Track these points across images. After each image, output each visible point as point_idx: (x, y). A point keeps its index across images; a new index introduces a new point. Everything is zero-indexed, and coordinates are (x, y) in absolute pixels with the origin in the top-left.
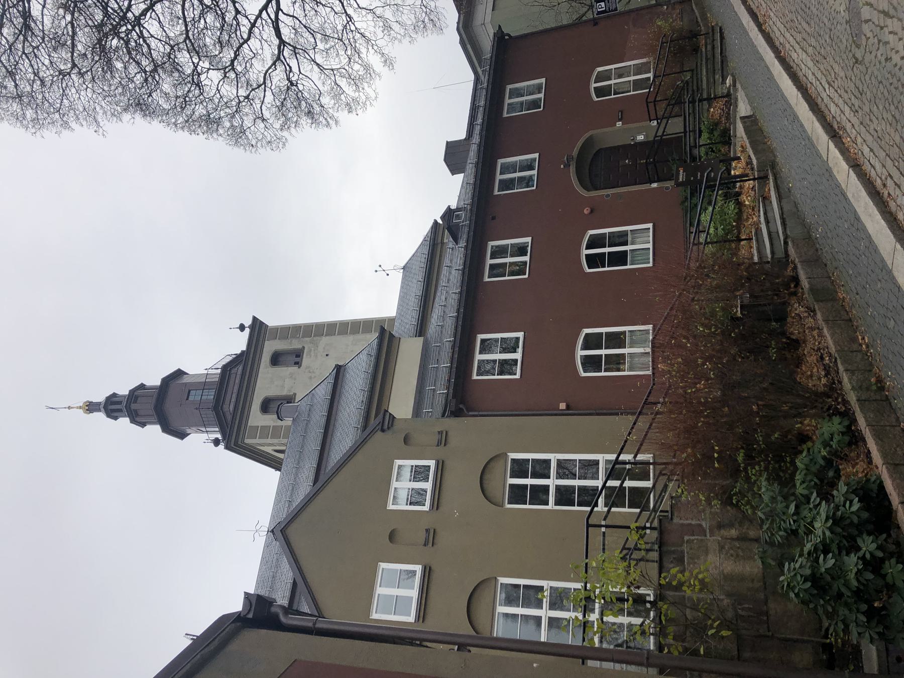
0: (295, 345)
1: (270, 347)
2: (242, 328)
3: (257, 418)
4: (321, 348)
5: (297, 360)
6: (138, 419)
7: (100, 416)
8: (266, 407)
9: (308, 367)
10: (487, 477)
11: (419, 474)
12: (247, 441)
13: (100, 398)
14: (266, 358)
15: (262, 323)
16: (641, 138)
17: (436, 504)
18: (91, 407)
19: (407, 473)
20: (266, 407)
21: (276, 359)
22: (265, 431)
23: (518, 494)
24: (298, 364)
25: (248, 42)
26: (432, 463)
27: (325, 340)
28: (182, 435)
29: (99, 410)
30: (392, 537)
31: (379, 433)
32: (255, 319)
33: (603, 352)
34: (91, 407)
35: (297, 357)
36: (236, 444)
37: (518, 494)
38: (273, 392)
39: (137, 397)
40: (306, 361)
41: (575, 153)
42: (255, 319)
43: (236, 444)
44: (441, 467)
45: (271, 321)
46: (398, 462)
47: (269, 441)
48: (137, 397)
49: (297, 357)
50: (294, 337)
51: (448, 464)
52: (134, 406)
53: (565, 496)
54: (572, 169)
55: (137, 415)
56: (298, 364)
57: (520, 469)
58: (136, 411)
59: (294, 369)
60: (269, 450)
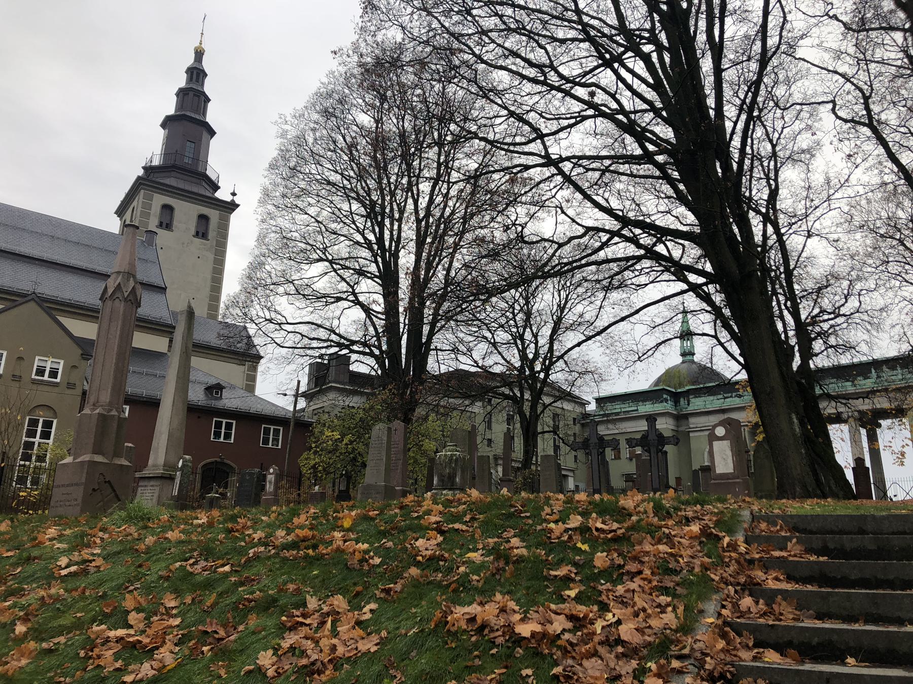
0: (212, 234)
1: (214, 215)
2: (234, 194)
3: (159, 200)
6: (182, 94)
7: (190, 60)
8: (168, 209)
11: (53, 374)
12: (142, 191)
13: (206, 65)
15: (234, 210)
16: (803, 451)
17: (34, 382)
18: (199, 54)
19: (55, 366)
21: (203, 218)
22: (147, 206)
23: (34, 423)
24: (197, 234)
25: (192, 378)
26: (58, 380)
27: (211, 256)
29: (196, 60)
30: (20, 358)
31: (80, 352)
32: (238, 206)
33: (223, 431)
34: (199, 54)
35: (202, 233)
37: (34, 423)
38: (177, 213)
39: (199, 97)
41: (226, 461)
42: (238, 206)
45: (235, 218)
46: (62, 362)
48: (199, 97)
49: (202, 233)
50: (219, 233)
51: (56, 389)
52: (191, 94)
56: (197, 234)
57: (48, 424)
59: (193, 232)
60: (135, 203)
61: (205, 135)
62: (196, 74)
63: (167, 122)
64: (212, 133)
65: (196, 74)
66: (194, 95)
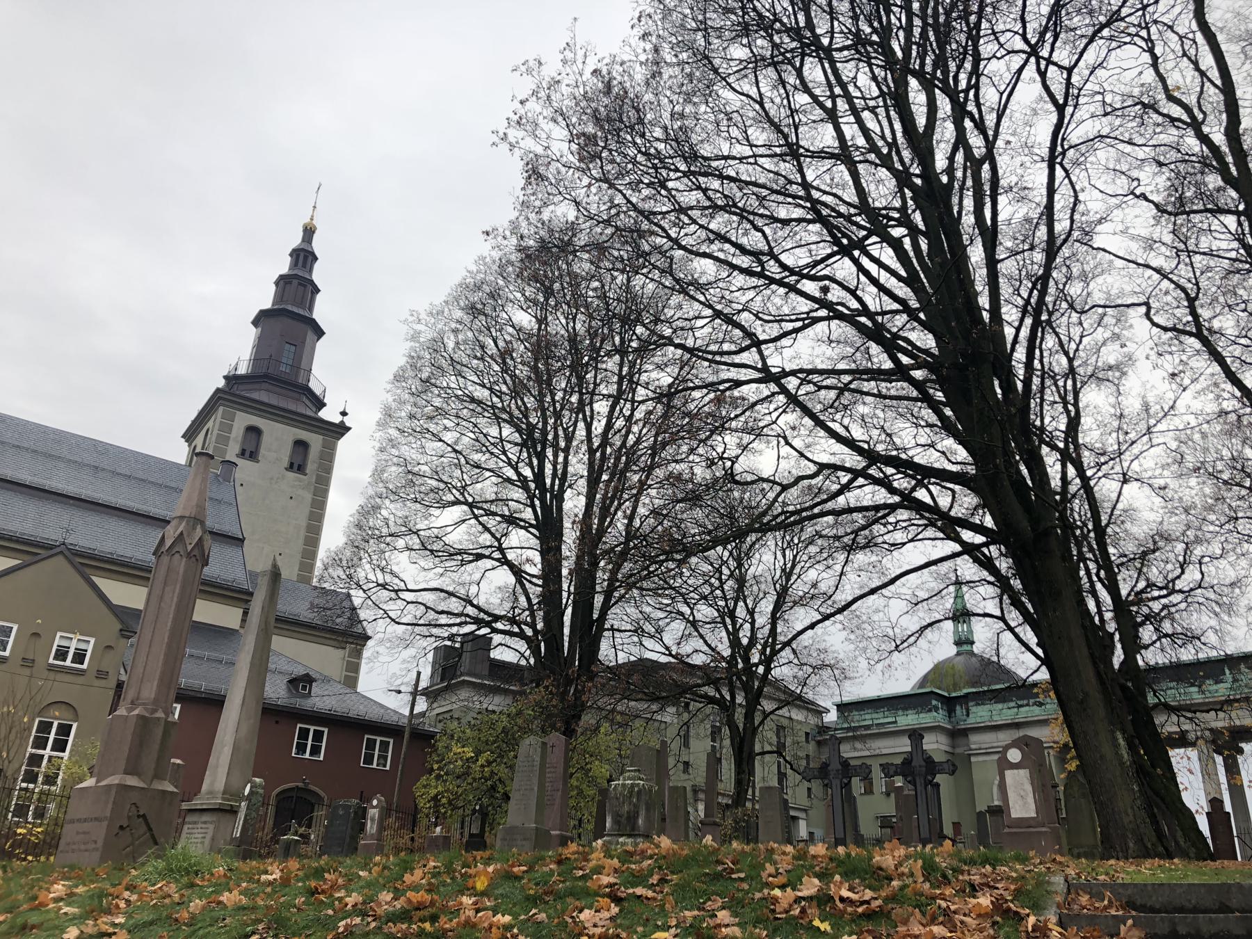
0: (311, 467)
1: (315, 441)
3: (243, 420)
4: (300, 492)
5: (296, 467)
6: (283, 281)
7: (296, 240)
9: (283, 477)
10: (64, 706)
12: (221, 408)
13: (317, 246)
14: (304, 435)
15: (343, 435)
16: (1136, 788)
17: (52, 668)
18: (309, 232)
19: (82, 646)
20: (254, 431)
21: (301, 445)
22: (226, 428)
23: (45, 727)
24: (291, 467)
27: (308, 496)
28: (255, 323)
29: (303, 240)
31: (119, 626)
32: (349, 429)
34: (309, 232)
35: (297, 466)
36: (220, 398)
37: (45, 727)
38: (266, 439)
40: (291, 475)
42: (349, 429)
43: (220, 398)
44: (82, 673)
45: (343, 444)
46: (92, 641)
47: (217, 426)
48: (305, 286)
49: (297, 466)
50: (320, 465)
51: (80, 680)
53: (36, 760)
54: (300, 785)
55: (286, 283)
56: (291, 467)
57: (65, 730)
58: (290, 283)
61: (310, 335)
62: (304, 257)
63: (262, 318)
64: (320, 333)
65: (304, 257)
66: (300, 284)
